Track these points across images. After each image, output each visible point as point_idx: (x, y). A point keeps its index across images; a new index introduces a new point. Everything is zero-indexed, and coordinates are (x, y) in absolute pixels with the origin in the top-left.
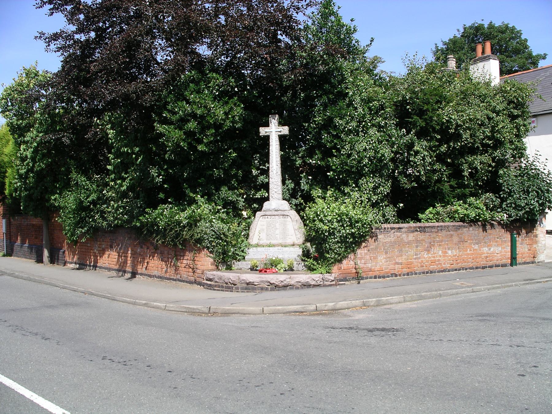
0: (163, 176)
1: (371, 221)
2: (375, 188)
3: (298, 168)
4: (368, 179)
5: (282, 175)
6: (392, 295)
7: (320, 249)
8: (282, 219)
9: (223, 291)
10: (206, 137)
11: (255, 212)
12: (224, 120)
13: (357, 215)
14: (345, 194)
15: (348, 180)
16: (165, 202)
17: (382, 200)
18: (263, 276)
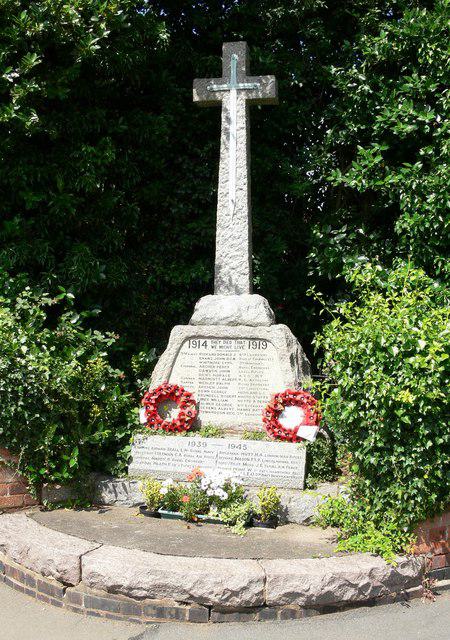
8: (247, 350)
9: (29, 593)
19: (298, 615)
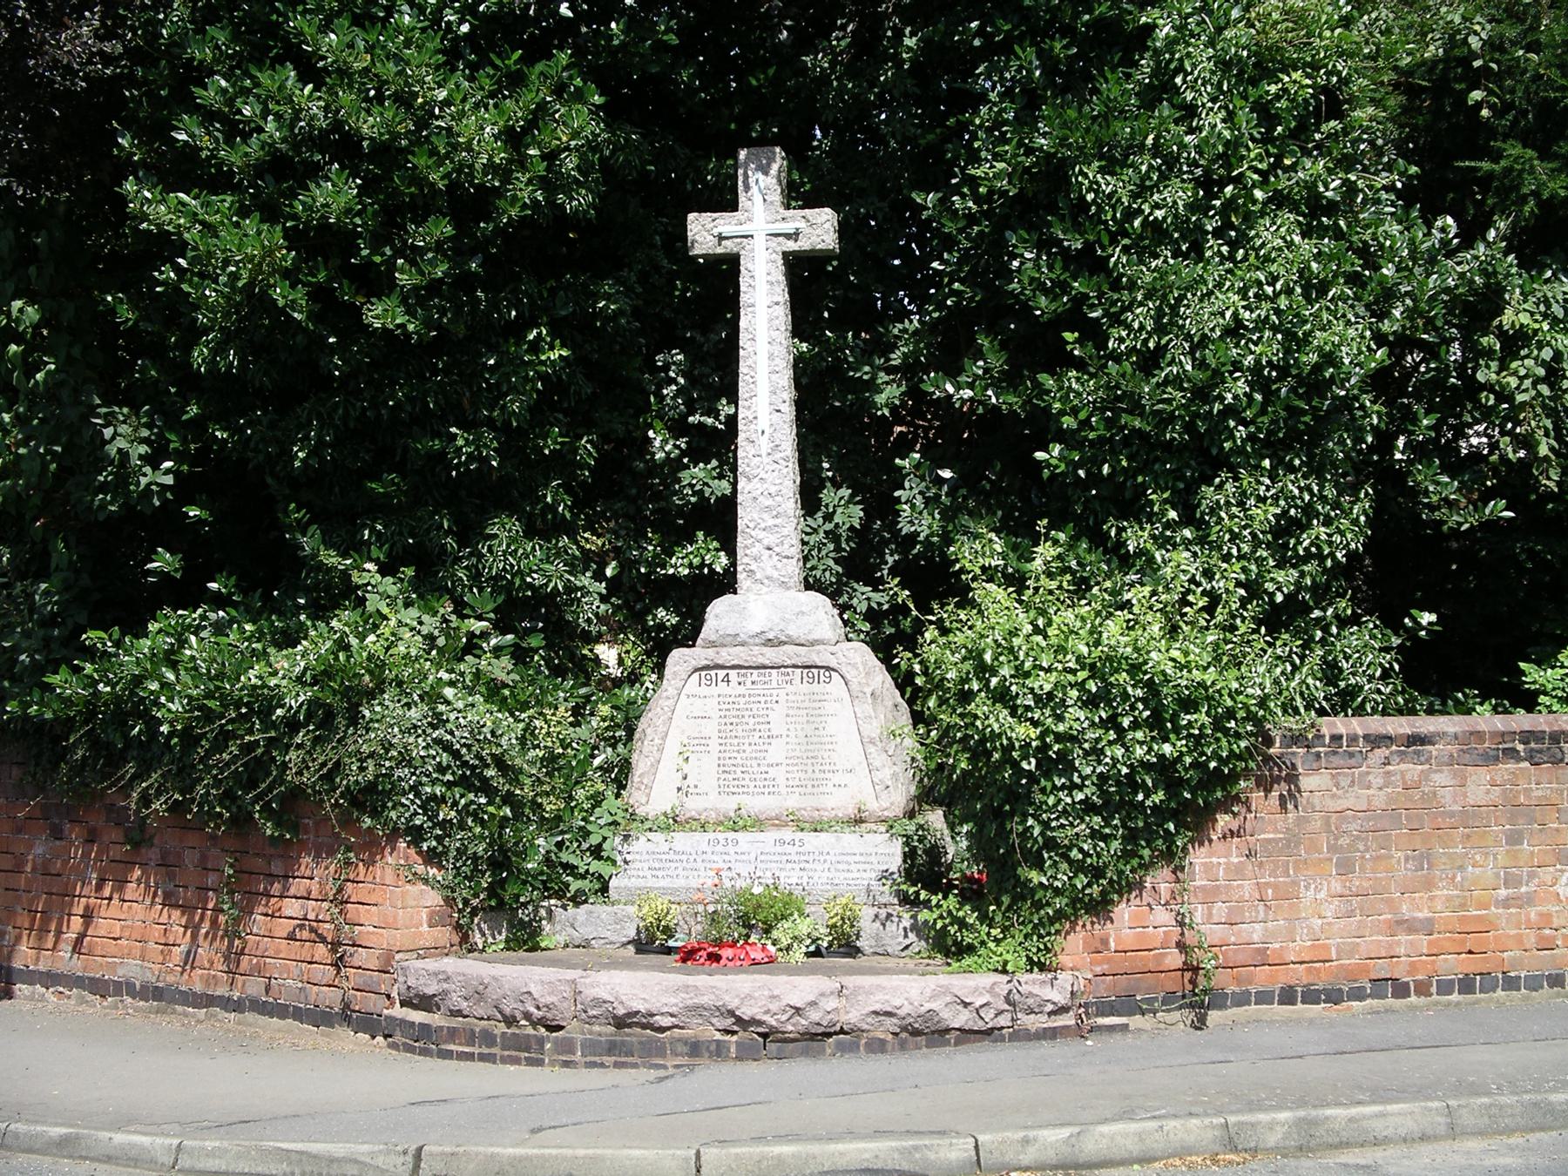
0: (178, 457)
1: (1263, 702)
2: (1286, 528)
3: (884, 425)
4: (1247, 480)
5: (802, 462)
6: (1380, 1095)
7: (1002, 840)
8: (799, 686)
10: (413, 263)
11: (659, 647)
12: (505, 173)
13: (1186, 666)
14: (1125, 561)
15: (1144, 486)
16: (185, 592)
17: (1322, 594)
18: (701, 980)
19: (889, 1047)
